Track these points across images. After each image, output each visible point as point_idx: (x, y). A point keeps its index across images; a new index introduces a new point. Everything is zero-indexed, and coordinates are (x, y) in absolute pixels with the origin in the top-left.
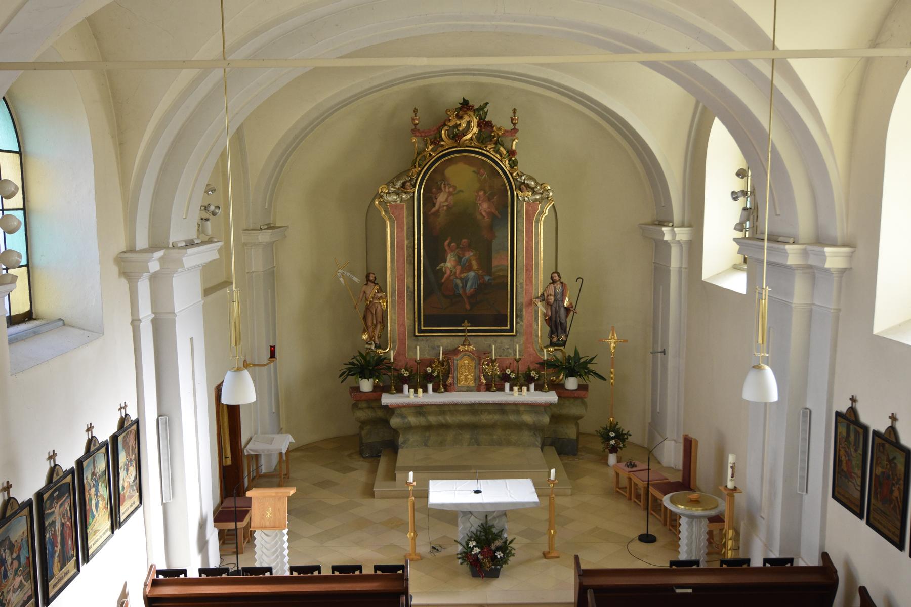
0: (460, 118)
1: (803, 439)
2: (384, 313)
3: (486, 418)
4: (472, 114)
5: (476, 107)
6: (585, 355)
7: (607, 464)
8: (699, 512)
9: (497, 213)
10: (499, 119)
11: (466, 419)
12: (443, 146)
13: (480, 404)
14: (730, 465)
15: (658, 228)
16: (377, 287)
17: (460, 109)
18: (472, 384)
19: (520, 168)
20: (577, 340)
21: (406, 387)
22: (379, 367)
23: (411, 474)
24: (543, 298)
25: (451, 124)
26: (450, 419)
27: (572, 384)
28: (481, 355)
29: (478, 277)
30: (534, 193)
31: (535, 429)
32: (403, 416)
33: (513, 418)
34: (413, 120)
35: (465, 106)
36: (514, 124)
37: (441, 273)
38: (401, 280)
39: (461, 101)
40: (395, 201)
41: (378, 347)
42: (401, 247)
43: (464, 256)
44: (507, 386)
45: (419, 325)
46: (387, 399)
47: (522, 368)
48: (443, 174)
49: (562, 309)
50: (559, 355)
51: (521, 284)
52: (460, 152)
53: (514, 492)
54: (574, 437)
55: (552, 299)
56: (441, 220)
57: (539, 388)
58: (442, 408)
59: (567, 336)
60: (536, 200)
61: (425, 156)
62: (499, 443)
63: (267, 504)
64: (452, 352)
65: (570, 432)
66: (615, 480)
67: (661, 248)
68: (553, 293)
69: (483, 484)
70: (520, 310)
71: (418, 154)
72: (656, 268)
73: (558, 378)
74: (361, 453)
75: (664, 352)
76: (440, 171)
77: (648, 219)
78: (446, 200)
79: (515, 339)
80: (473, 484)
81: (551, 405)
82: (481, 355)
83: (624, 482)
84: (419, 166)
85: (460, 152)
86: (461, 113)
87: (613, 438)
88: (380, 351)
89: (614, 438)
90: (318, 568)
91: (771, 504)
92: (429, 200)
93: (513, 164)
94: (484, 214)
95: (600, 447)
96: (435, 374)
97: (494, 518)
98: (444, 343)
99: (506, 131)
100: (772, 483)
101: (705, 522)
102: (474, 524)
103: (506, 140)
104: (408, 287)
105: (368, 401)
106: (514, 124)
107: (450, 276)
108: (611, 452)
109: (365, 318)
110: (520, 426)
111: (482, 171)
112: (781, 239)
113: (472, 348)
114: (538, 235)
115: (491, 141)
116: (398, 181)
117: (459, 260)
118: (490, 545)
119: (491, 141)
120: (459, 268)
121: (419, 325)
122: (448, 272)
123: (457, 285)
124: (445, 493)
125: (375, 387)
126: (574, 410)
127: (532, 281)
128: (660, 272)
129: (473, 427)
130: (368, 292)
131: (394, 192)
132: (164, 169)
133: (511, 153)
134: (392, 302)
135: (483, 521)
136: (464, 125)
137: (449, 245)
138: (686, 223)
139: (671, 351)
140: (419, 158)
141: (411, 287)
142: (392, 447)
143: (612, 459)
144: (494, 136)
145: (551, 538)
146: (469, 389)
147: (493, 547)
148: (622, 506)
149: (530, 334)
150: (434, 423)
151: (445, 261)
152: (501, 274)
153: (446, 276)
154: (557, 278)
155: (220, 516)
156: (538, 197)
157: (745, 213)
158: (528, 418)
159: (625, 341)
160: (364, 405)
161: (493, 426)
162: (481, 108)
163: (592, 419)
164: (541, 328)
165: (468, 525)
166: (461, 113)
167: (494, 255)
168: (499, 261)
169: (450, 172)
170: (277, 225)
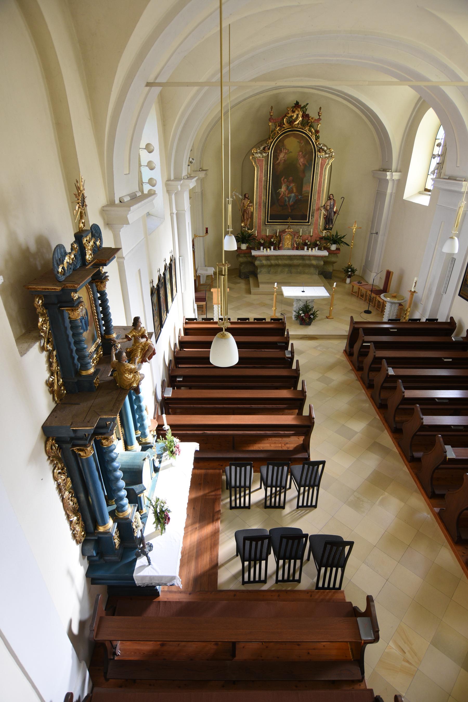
0: (293, 112)
1: (449, 271)
2: (252, 213)
3: (296, 262)
4: (299, 109)
5: (302, 106)
6: (341, 234)
7: (345, 283)
8: (396, 301)
9: (307, 164)
10: (312, 112)
11: (287, 262)
12: (284, 127)
13: (294, 256)
14: (415, 282)
15: (384, 172)
16: (249, 201)
17: (294, 107)
18: (290, 247)
19: (321, 140)
20: (338, 226)
21: (262, 248)
22: (250, 239)
23: (276, 284)
24: (325, 207)
25: (289, 115)
26: (280, 262)
27: (333, 247)
28: (295, 234)
29: (296, 196)
30: (326, 153)
31: (316, 267)
32: (260, 261)
33: (307, 262)
34: (270, 113)
35: (297, 105)
36: (320, 116)
37: (279, 194)
38: (260, 198)
39: (295, 103)
40: (260, 157)
41: (248, 229)
42: (261, 181)
43: (290, 185)
44: (306, 248)
45: (268, 219)
46: (254, 253)
47: (313, 240)
48: (283, 143)
49: (333, 212)
50: (329, 234)
51: (315, 200)
52: (292, 131)
53: (317, 292)
54: (331, 271)
55: (328, 207)
56: (281, 167)
57: (320, 249)
58: (277, 257)
59: (333, 226)
60: (326, 157)
61: (275, 133)
62: (300, 273)
63: (216, 294)
64: (283, 231)
65: (330, 269)
66: (351, 289)
67: (383, 182)
68: (329, 205)
69: (305, 288)
70: (313, 213)
71: (272, 132)
72: (377, 192)
73: (327, 244)
74: (240, 277)
75: (377, 233)
76: (282, 141)
77: (377, 168)
78: (284, 157)
79: (310, 227)
80: (301, 288)
81: (325, 257)
82: (295, 234)
83: (356, 289)
84: (272, 138)
85: (292, 131)
86: (294, 109)
87: (350, 271)
88: (249, 231)
89: (349, 272)
90: (248, 319)
91: (428, 298)
92: (276, 157)
93: (317, 138)
94: (301, 164)
95: (343, 275)
96: (275, 242)
97: (310, 302)
98: (278, 228)
99: (316, 120)
100: (430, 290)
101: (397, 305)
102: (301, 304)
103: (315, 125)
104: (263, 201)
105: (245, 254)
106: (320, 116)
107: (283, 195)
108: (348, 278)
109: (243, 215)
110: (310, 266)
111: (302, 142)
112: (458, 179)
113: (292, 230)
114: (325, 175)
115: (308, 125)
116: (261, 145)
117: (288, 187)
118: (308, 313)
119: (308, 125)
120: (287, 191)
121: (268, 219)
122: (282, 194)
123: (286, 200)
124: (290, 292)
125: (248, 248)
126: (333, 259)
127: (320, 200)
128: (379, 195)
129: (290, 266)
130: (245, 203)
131: (259, 152)
132: (180, 139)
133: (317, 132)
134: (256, 208)
135: (305, 303)
136: (295, 116)
137: (284, 180)
138: (398, 170)
139: (381, 233)
140: (271, 134)
141: (265, 201)
142: (255, 274)
143: (348, 280)
144: (309, 123)
145: (330, 311)
146: (289, 249)
147: (309, 314)
148: (354, 299)
149: (317, 224)
150: (273, 264)
151: (281, 188)
152: (306, 195)
153: (281, 195)
154: (332, 197)
155: (198, 299)
156: (327, 156)
157: (438, 165)
158: (314, 262)
159: (360, 228)
160: (242, 255)
161: (298, 266)
162: (305, 107)
163: (340, 263)
164: (321, 221)
165: (299, 305)
166: (294, 109)
167: (304, 185)
168: (306, 188)
169: (287, 142)
170: (204, 169)
